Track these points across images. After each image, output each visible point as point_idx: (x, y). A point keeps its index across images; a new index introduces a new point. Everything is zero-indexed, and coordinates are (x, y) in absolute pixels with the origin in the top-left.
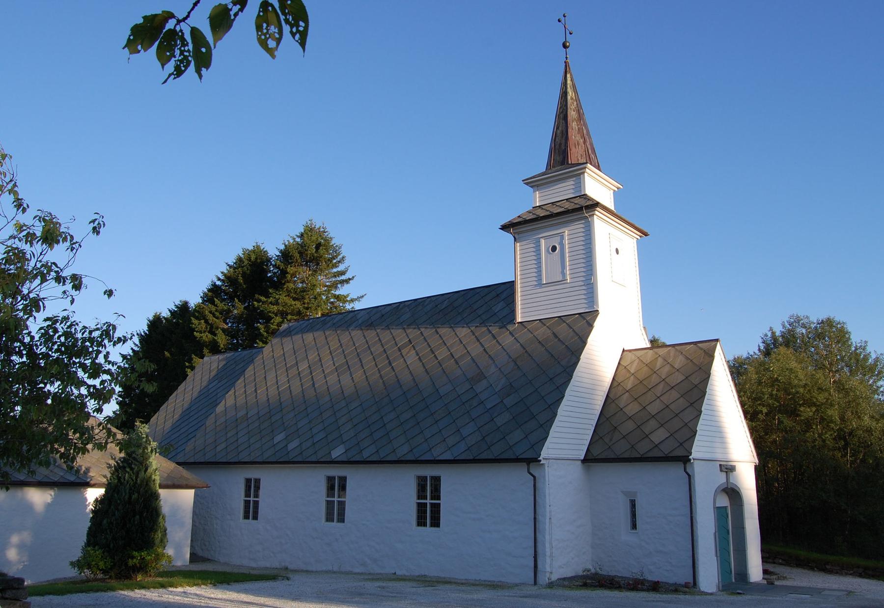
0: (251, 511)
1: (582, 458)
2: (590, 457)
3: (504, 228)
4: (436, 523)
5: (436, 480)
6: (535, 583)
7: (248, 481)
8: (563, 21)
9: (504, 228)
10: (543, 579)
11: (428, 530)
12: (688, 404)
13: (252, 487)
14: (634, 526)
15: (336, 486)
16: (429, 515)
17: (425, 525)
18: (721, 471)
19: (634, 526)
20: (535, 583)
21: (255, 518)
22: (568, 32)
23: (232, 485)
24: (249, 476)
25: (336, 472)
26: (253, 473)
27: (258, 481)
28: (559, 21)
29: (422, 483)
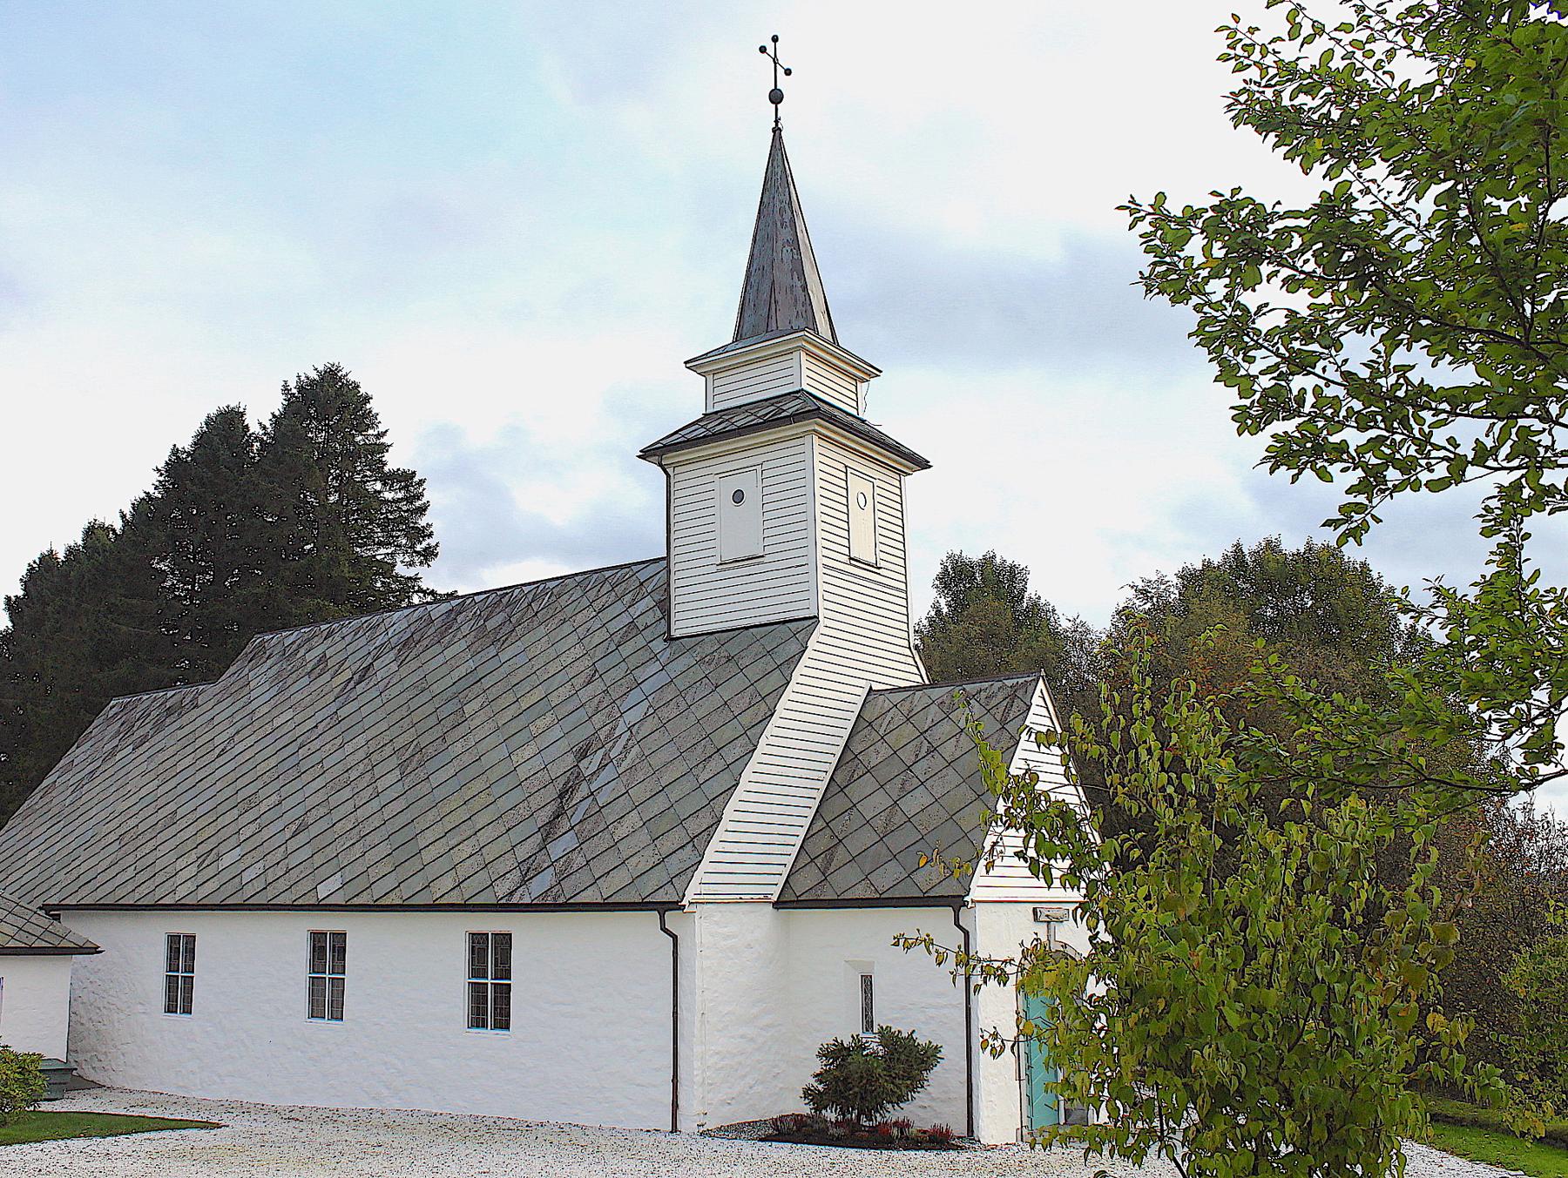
0: (179, 997)
1: (775, 893)
2: (789, 897)
3: (645, 454)
4: (503, 1023)
5: (504, 940)
6: (674, 1129)
7: (173, 940)
8: (770, 50)
9: (645, 454)
10: (687, 1124)
11: (489, 1035)
12: (974, 797)
13: (181, 951)
14: (867, 982)
15: (328, 953)
16: (490, 1006)
17: (484, 1026)
18: (1036, 919)
19: (867, 982)
20: (674, 1129)
21: (187, 1010)
22: (780, 71)
23: (137, 949)
24: (175, 930)
25: (328, 923)
26: (182, 924)
27: (191, 939)
28: (763, 50)
29: (478, 942)
